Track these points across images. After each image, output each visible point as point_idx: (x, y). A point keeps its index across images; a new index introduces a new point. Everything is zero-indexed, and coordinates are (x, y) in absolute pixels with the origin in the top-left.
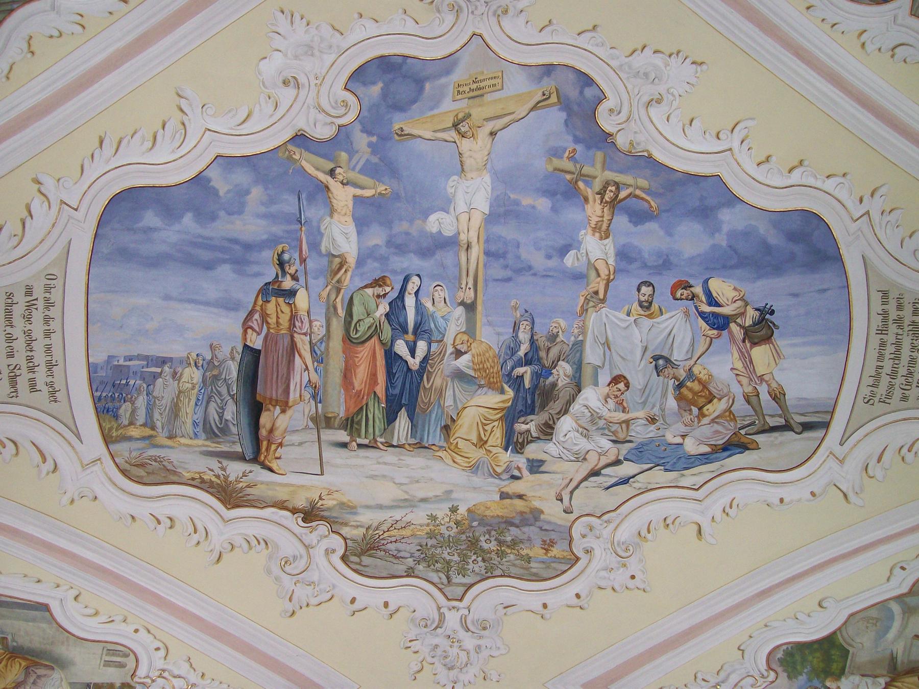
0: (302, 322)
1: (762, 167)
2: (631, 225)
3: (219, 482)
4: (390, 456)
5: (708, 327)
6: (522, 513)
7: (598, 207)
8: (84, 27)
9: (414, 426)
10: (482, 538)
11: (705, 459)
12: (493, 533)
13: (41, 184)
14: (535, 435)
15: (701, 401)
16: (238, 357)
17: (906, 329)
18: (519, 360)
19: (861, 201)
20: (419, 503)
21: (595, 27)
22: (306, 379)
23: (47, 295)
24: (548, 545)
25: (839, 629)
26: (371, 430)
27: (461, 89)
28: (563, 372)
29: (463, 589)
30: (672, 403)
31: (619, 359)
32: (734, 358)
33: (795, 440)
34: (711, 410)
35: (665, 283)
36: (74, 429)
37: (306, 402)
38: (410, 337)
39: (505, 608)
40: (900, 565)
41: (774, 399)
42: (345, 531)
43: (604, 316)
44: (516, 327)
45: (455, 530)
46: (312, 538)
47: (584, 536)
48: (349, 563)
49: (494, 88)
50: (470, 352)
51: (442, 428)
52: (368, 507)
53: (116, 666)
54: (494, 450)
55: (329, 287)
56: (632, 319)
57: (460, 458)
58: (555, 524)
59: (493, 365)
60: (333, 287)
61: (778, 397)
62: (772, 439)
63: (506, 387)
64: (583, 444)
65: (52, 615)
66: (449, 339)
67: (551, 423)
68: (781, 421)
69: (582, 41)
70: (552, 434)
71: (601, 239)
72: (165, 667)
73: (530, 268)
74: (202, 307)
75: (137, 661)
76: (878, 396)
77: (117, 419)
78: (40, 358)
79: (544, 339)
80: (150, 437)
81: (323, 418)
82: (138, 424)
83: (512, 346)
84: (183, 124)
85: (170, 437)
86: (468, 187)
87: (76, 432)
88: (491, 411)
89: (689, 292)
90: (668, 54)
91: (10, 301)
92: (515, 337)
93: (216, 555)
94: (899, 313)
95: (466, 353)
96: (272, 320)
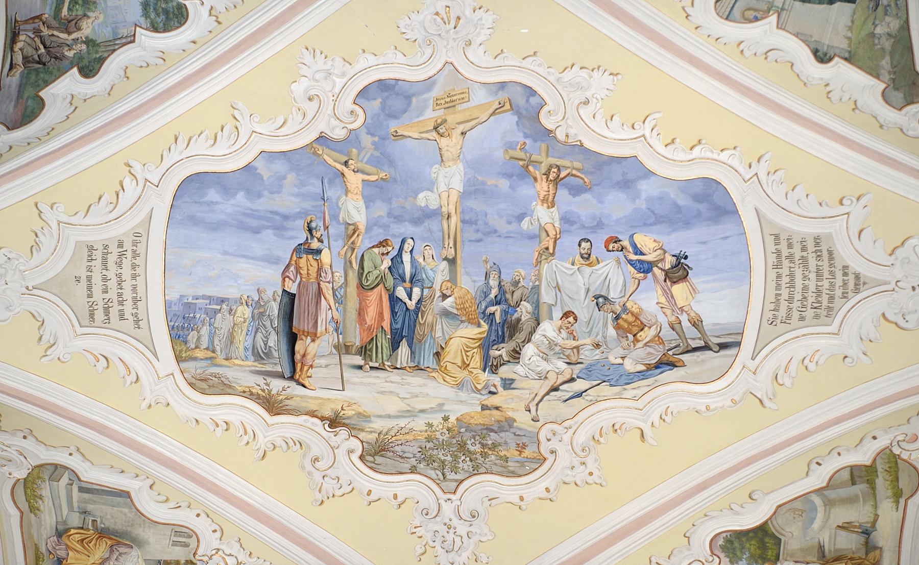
0: (326, 274)
1: (669, 147)
2: (571, 197)
3: (264, 395)
4: (395, 376)
5: (636, 272)
6: (499, 421)
7: (545, 185)
8: (165, 60)
9: (413, 353)
10: (468, 442)
11: (642, 375)
12: (477, 438)
13: (131, 167)
14: (506, 359)
15: (635, 330)
16: (279, 299)
17: (797, 262)
18: (491, 301)
19: (750, 167)
20: (419, 414)
21: (535, 53)
22: (330, 317)
23: (135, 248)
24: (521, 448)
25: (770, 518)
26: (380, 356)
27: (439, 102)
28: (525, 310)
29: (456, 484)
30: (611, 332)
31: (568, 298)
32: (659, 294)
33: (714, 358)
34: (643, 336)
35: (599, 240)
36: (152, 349)
37: (331, 333)
38: (408, 285)
39: (489, 500)
40: (816, 461)
41: (693, 325)
42: (362, 435)
43: (554, 265)
44: (487, 276)
45: (447, 435)
46: (335, 441)
47: (549, 440)
48: (365, 462)
49: (464, 101)
50: (453, 296)
51: (434, 355)
52: (380, 416)
53: (182, 546)
54: (475, 371)
55: (346, 247)
56: (576, 267)
57: (449, 377)
58: (526, 430)
59: (471, 305)
60: (349, 247)
61: (697, 323)
62: (695, 358)
63: (482, 322)
64: (544, 366)
65: (132, 501)
66: (437, 286)
67: (518, 349)
68: (702, 343)
69: (527, 63)
70: (519, 358)
71: (548, 208)
72: (221, 547)
73: (496, 231)
74: (251, 261)
75: (198, 541)
76: (780, 318)
77: (186, 344)
78: (128, 295)
79: (509, 284)
80: (211, 358)
81: (342, 345)
82: (202, 348)
83: (485, 290)
84: (237, 128)
85: (227, 359)
86: (446, 173)
87: (154, 351)
88: (471, 340)
89: (618, 245)
90: (591, 69)
91: (106, 251)
92: (487, 284)
93: (261, 453)
94: (790, 250)
95: (450, 296)
96: (304, 272)
